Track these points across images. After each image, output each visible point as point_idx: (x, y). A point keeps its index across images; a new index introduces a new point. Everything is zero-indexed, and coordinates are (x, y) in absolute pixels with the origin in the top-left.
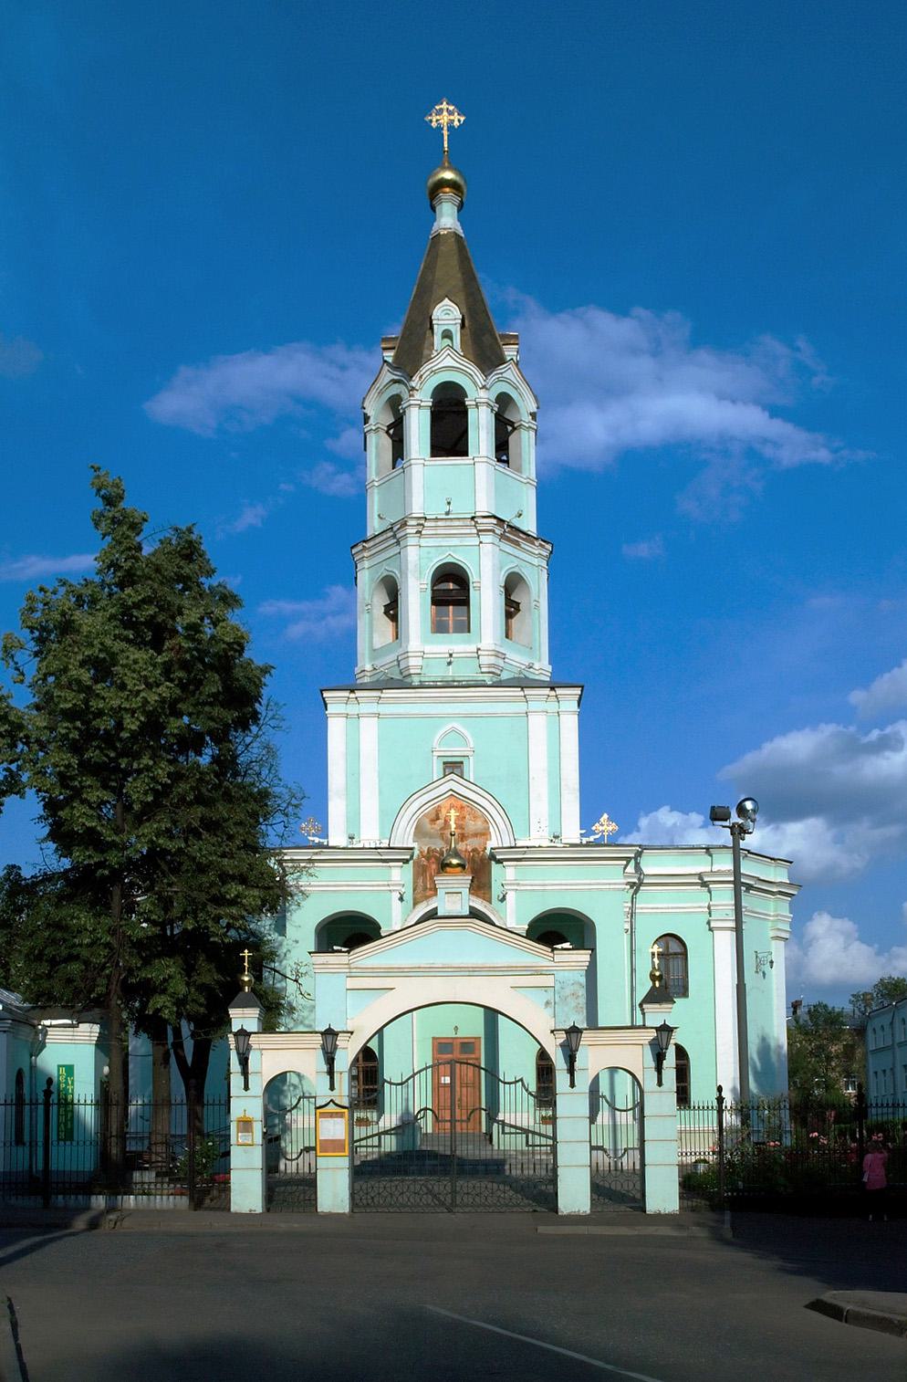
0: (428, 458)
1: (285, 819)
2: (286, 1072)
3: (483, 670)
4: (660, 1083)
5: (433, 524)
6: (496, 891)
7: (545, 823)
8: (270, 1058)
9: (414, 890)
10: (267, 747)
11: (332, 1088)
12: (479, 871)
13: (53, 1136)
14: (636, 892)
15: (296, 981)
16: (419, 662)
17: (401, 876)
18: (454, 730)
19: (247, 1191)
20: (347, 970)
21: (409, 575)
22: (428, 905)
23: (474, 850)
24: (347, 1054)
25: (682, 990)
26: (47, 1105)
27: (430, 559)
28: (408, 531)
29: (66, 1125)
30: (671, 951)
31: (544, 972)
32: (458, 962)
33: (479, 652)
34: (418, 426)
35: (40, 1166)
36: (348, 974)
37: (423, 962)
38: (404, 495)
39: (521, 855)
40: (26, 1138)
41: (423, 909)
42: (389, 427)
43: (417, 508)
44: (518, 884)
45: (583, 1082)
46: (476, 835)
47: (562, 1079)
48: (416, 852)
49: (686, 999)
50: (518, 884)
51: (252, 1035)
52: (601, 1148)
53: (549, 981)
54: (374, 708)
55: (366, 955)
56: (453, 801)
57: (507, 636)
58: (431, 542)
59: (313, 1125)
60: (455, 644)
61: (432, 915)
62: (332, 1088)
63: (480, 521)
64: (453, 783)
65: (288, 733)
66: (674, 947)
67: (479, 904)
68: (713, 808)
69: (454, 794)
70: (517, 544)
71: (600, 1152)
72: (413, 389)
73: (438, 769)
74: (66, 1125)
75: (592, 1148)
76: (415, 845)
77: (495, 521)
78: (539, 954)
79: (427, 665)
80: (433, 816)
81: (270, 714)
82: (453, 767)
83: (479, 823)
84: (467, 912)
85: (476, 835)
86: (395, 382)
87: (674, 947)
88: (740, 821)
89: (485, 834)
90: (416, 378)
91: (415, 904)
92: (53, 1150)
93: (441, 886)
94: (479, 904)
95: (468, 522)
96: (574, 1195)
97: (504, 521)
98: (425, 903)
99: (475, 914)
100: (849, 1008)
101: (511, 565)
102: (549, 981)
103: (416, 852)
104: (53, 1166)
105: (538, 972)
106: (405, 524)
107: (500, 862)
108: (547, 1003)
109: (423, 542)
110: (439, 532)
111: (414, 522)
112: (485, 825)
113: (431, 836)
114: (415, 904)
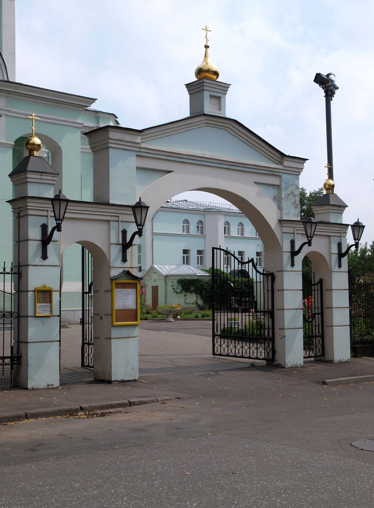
20: (138, 150)
31: (275, 173)
36: (138, 154)
44: (9, 111)
50: (9, 111)
53: (274, 181)
62: (124, 260)
93: (207, 88)
102: (274, 181)
105: (271, 172)
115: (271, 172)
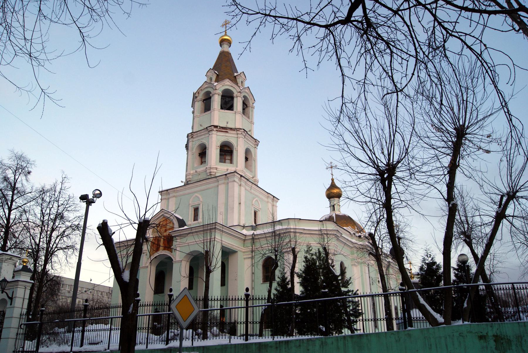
3: (208, 174)
5: (196, 133)
18: (196, 196)
22: (153, 256)
33: (207, 169)
60: (202, 168)
63: (208, 128)
70: (227, 132)
77: (213, 127)
79: (192, 177)
83: (171, 225)
89: (173, 228)
95: (206, 130)
109: (194, 140)
110: (199, 135)
111: (190, 135)
112: (173, 225)
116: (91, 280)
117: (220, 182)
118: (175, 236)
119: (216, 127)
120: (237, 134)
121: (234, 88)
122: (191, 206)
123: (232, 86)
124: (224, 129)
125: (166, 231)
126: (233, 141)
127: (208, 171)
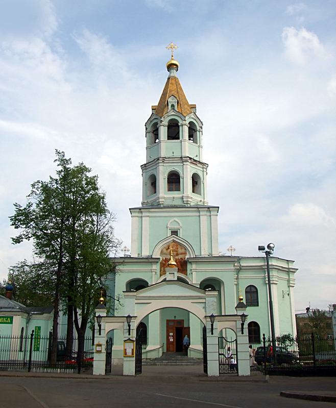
0: (167, 140)
1: (116, 249)
2: (113, 330)
4: (243, 333)
6: (189, 272)
7: (207, 250)
8: (107, 326)
9: (160, 271)
10: (111, 227)
11: (129, 334)
12: (183, 266)
13: (33, 349)
14: (238, 272)
15: (118, 300)
16: (163, 200)
17: (156, 267)
18: (175, 221)
19: (99, 367)
21: (160, 175)
23: (181, 259)
24: (134, 325)
25: (257, 304)
26: (32, 339)
27: (167, 170)
28: (160, 161)
29: (37, 346)
30: (252, 291)
32: (173, 295)
34: (163, 131)
35: (28, 359)
37: (161, 295)
38: (159, 150)
39: (199, 260)
40: (23, 349)
41: (163, 278)
42: (154, 131)
43: (163, 155)
45: (216, 333)
46: (182, 254)
47: (209, 334)
48: (161, 259)
49: (257, 307)
51: (103, 319)
52: (223, 354)
53: (204, 301)
54: (148, 214)
55: (144, 293)
56: (174, 243)
57: (193, 192)
58: (167, 164)
59: (235, 348)
60: (176, 194)
61: (165, 280)
62: (129, 334)
64: (174, 238)
65: (29, 240)
66: (253, 289)
67: (182, 276)
68: (259, 247)
69: (174, 241)
71: (222, 356)
72: (161, 121)
73: (169, 234)
74: (37, 346)
75: (219, 354)
76: (161, 257)
78: (201, 292)
80: (167, 248)
81: (112, 217)
82: (175, 233)
83: (183, 251)
84: (176, 279)
85: (182, 254)
86: (155, 119)
87: (253, 289)
88: (268, 250)
89: (185, 254)
90: (163, 118)
91: (161, 276)
92: (33, 353)
94: (182, 276)
96: (213, 369)
97: (191, 158)
98: (164, 276)
99: (180, 280)
100: (327, 309)
101: (194, 171)
102: (204, 301)
103: (161, 259)
104: (32, 359)
105: (200, 298)
106: (158, 159)
107: (190, 262)
108: (203, 308)
109: (165, 165)
113: (166, 254)
114: (161, 276)
115: (200, 298)
116: (175, 317)
117: (201, 213)
118: (190, 262)
119: (190, 158)
120: (203, 168)
121: (197, 122)
122: (170, 229)
123: (195, 120)
124: (195, 162)
125: (177, 255)
126: (200, 174)
127: (184, 199)
